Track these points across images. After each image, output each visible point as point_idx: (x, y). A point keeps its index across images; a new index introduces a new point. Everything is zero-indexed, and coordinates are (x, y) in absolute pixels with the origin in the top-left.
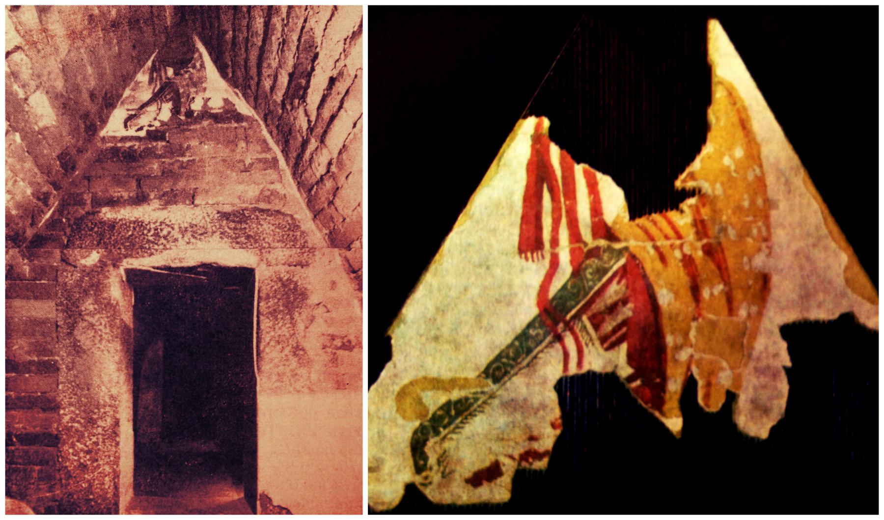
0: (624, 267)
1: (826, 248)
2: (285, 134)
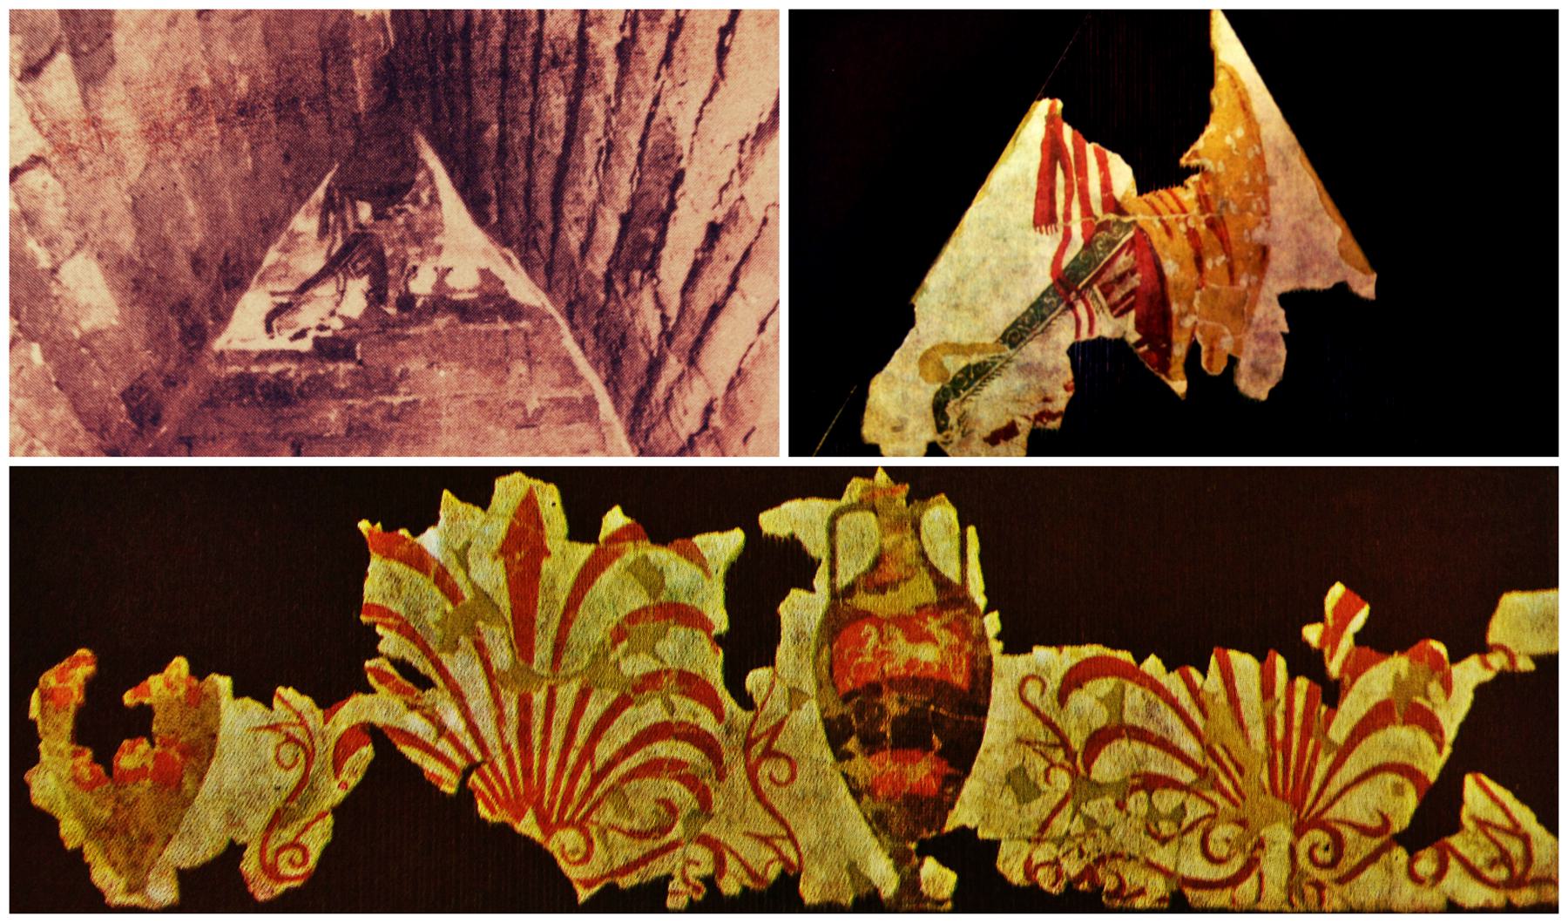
0: (1132, 239)
1: (1321, 222)
2: (612, 347)
